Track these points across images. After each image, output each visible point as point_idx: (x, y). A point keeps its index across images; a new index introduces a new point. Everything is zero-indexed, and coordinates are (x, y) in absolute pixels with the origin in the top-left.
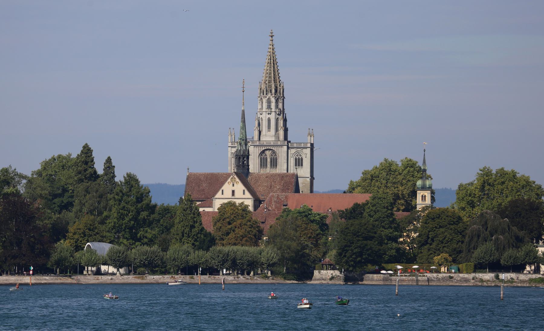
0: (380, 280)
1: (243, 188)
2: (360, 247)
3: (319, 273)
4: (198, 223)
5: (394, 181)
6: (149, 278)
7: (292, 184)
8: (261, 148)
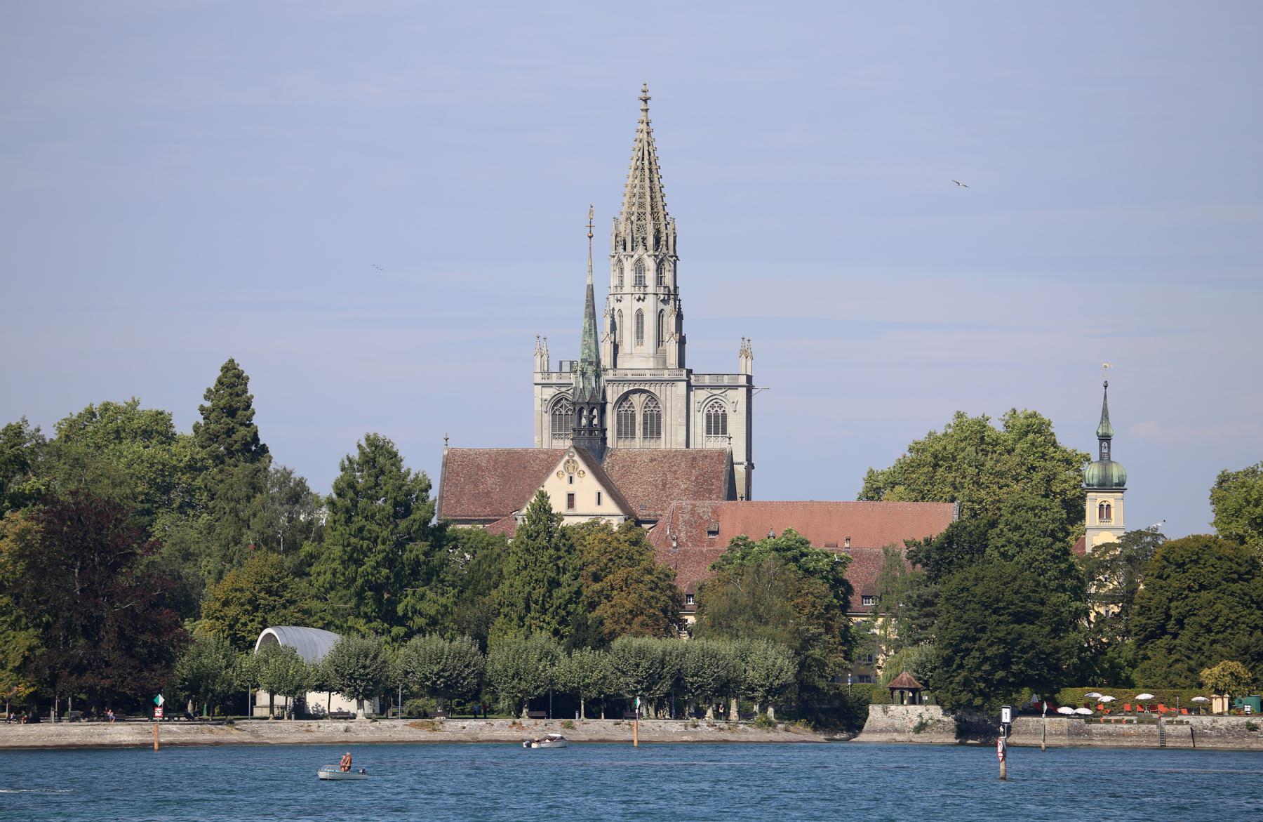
0: (1061, 734)
1: (598, 487)
2: (1001, 641)
3: (885, 712)
4: (568, 574)
5: (997, 469)
6: (450, 726)
7: (718, 478)
8: (620, 388)
